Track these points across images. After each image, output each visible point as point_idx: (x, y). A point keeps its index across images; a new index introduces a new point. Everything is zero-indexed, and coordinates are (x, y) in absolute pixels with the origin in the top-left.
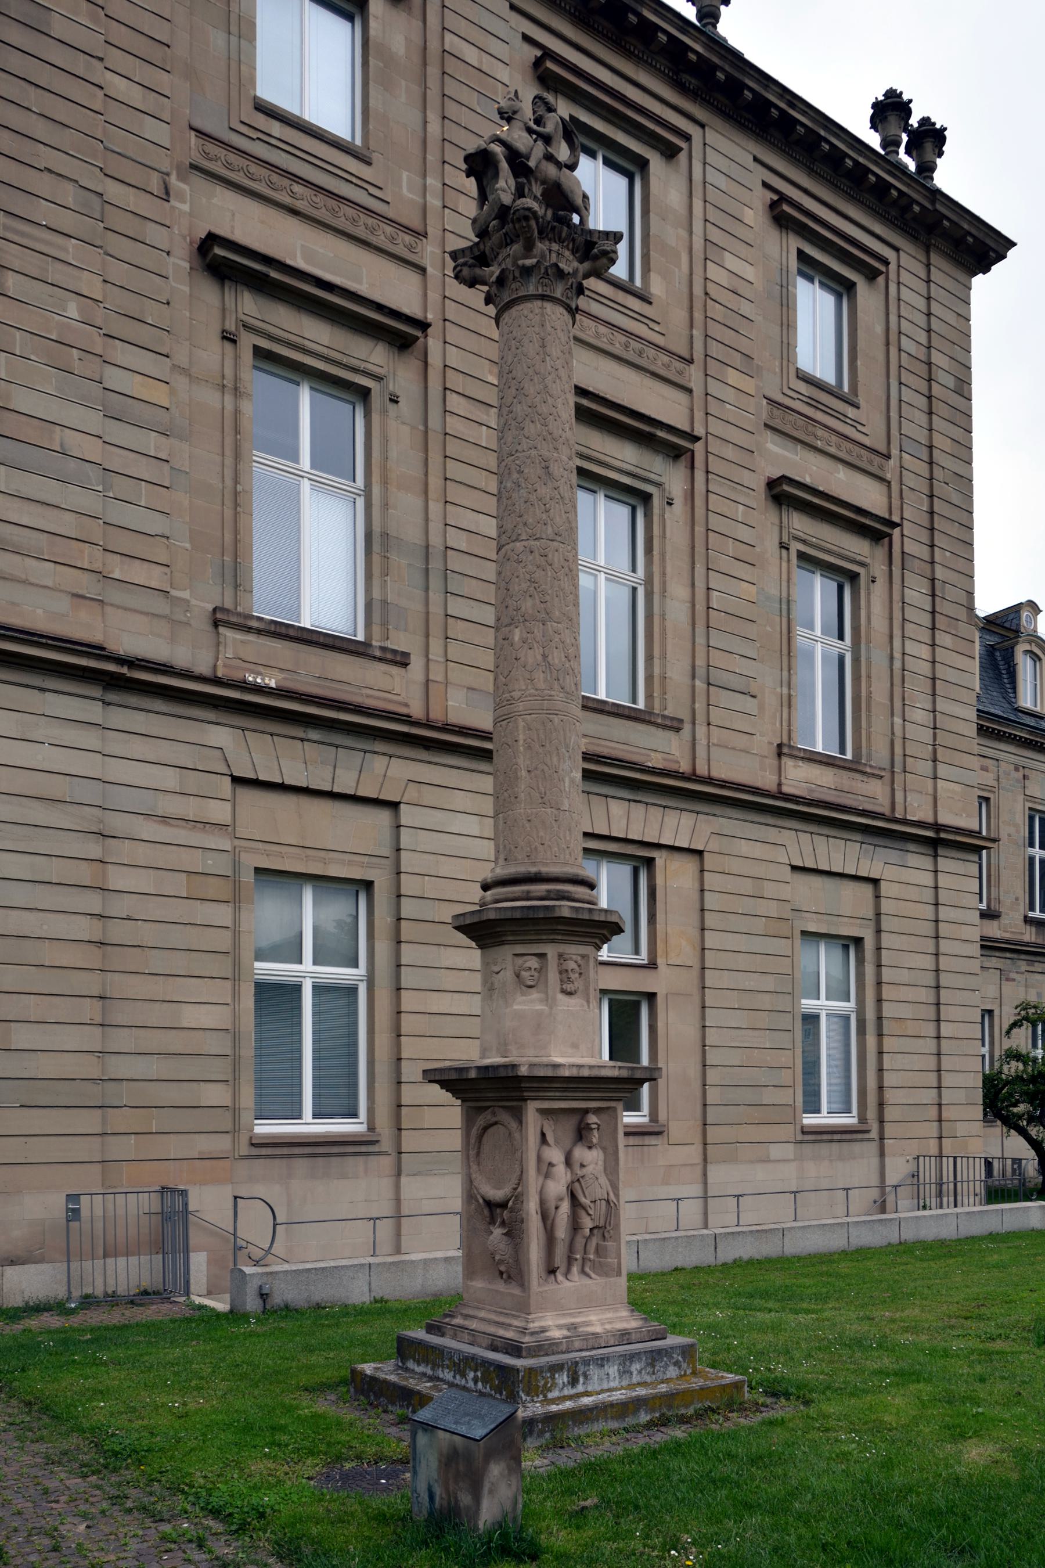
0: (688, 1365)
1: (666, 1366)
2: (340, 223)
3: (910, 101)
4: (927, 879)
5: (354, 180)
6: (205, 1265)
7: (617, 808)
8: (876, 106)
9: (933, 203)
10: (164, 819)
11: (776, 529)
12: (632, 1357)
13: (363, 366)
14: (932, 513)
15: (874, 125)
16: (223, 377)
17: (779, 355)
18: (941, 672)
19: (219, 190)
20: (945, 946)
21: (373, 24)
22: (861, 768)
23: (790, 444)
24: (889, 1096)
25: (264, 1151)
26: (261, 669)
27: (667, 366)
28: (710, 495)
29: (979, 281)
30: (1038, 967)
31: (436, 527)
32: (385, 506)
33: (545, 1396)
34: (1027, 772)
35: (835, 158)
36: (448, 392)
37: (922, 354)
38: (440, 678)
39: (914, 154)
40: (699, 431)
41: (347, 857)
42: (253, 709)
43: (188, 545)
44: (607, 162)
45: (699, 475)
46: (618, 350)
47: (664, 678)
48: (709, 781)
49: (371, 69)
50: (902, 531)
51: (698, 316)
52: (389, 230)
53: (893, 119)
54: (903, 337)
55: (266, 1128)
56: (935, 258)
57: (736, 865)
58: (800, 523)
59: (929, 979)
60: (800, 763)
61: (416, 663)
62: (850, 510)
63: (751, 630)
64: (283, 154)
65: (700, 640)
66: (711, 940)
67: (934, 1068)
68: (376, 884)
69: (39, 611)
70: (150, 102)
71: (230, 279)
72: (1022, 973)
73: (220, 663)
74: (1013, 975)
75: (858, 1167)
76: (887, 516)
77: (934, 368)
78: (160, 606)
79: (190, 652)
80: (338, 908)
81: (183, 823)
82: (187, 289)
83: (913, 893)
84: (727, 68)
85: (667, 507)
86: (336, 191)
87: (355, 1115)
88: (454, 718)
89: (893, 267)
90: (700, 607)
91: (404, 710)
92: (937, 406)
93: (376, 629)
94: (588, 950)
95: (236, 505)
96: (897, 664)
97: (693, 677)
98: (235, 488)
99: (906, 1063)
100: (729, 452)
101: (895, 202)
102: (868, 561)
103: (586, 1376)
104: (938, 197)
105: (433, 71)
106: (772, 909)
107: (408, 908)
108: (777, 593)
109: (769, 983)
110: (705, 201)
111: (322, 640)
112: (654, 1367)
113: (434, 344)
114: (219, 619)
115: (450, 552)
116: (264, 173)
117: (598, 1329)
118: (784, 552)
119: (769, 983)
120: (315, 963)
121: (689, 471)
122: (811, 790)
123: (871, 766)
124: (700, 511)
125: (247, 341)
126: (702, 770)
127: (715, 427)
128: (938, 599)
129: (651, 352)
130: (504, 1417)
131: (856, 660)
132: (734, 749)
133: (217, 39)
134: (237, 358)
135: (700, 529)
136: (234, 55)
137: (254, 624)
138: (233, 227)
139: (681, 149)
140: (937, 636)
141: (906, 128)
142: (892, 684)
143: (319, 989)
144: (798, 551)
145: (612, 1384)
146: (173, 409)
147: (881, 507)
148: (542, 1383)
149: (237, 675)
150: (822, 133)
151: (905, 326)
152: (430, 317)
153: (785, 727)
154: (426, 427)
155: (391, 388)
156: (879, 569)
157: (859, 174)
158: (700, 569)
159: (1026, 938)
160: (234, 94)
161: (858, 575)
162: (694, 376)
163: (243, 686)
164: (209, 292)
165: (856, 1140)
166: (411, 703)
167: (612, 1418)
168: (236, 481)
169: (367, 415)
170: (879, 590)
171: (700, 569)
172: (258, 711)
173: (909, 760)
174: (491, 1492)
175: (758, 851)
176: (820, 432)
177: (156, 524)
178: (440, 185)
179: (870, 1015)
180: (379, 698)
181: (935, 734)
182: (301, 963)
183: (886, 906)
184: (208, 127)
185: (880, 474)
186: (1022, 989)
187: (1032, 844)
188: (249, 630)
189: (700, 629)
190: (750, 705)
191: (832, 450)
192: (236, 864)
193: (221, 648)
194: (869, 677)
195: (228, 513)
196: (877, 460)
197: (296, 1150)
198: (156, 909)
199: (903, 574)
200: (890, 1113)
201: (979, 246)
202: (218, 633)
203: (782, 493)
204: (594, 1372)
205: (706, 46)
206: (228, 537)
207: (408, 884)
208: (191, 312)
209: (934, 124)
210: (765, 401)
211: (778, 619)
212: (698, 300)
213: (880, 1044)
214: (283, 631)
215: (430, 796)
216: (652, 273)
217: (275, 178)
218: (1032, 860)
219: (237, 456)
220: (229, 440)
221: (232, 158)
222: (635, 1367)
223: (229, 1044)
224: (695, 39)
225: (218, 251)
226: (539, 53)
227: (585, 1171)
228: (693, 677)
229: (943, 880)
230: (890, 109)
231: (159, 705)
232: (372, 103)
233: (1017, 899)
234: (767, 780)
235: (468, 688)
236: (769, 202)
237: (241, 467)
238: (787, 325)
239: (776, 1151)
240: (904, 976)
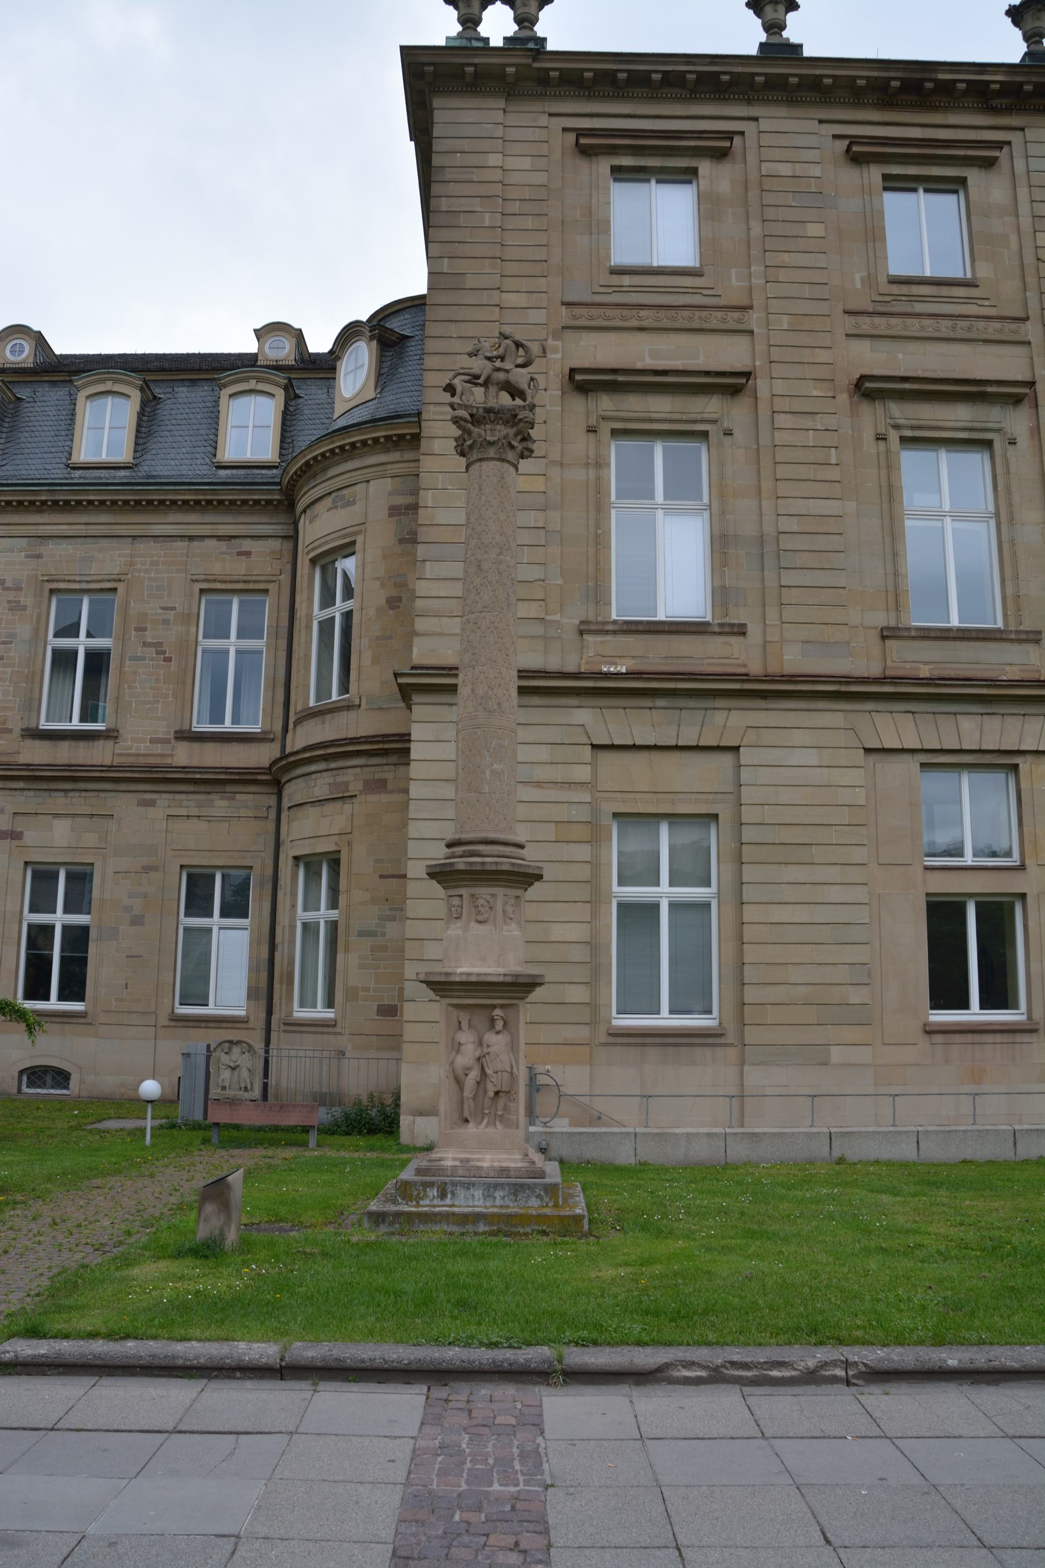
0: (550, 1199)
1: (528, 1197)
5: (690, 290)
7: (967, 724)
10: (539, 784)
12: (496, 1186)
16: (588, 458)
19: (584, 335)
21: (701, 183)
25: (620, 1040)
26: (617, 660)
33: (418, 1202)
41: (693, 796)
44: (926, 191)
46: (945, 333)
61: (754, 632)
68: (720, 816)
69: (450, 652)
71: (592, 391)
78: (538, 630)
80: (689, 835)
85: (1011, 448)
86: (676, 304)
87: (710, 1012)
88: (789, 669)
94: (518, 892)
95: (597, 544)
103: (453, 1194)
105: (753, 194)
112: (517, 1196)
114: (584, 630)
115: (781, 536)
116: (617, 312)
117: (485, 1165)
120: (671, 885)
121: (1033, 410)
125: (606, 428)
129: (981, 324)
130: (215, 1179)
137: (610, 627)
143: (673, 906)
145: (476, 1203)
148: (415, 1193)
149: (595, 668)
154: (758, 444)
155: (725, 425)
167: (453, 1223)
174: (205, 1220)
178: (763, 268)
182: (658, 885)
188: (607, 632)
192: (596, 812)
197: (648, 1040)
204: (461, 1192)
205: (1006, 73)
206: (591, 568)
207: (748, 814)
214: (634, 628)
215: (768, 737)
222: (499, 1194)
227: (489, 1050)
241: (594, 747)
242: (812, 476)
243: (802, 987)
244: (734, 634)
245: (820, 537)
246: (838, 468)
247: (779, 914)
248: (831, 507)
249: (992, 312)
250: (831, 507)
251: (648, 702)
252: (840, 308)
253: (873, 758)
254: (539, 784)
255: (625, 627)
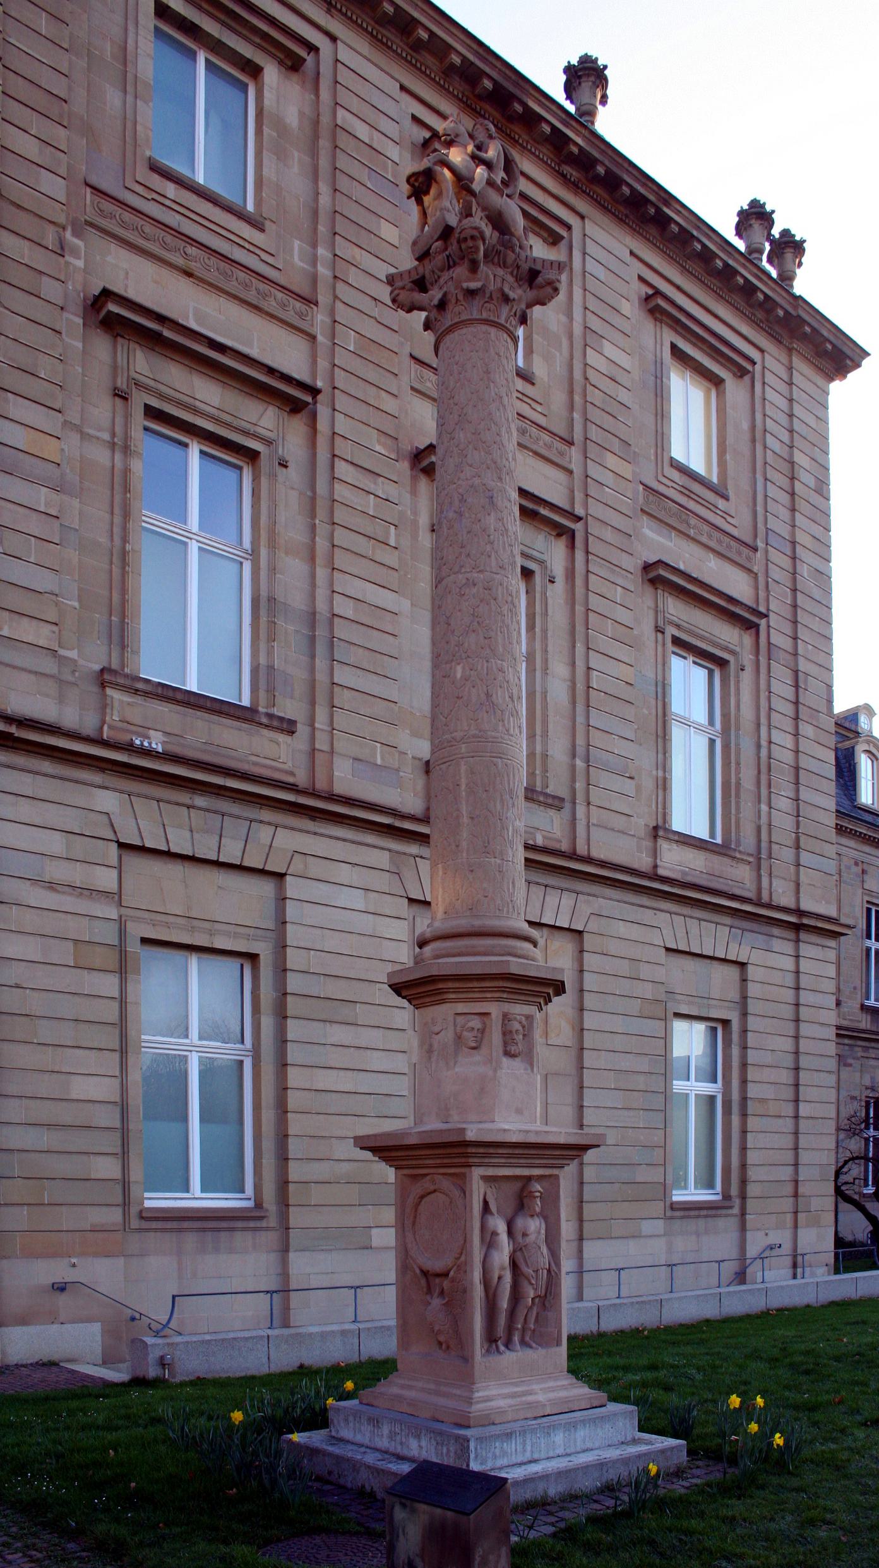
2: (232, 287)
3: (773, 212)
4: (788, 964)
5: (246, 245)
6: (99, 1336)
8: (742, 213)
9: (796, 307)
10: (51, 886)
11: (651, 614)
13: (252, 429)
14: (795, 606)
15: (739, 232)
17: (653, 442)
18: (804, 762)
20: (804, 1029)
22: (733, 854)
23: (665, 531)
24: (752, 1174)
25: (154, 1225)
27: (549, 447)
28: (590, 575)
29: (836, 388)
30: (872, 1053)
31: (321, 593)
32: (273, 570)
34: (865, 867)
35: (706, 256)
36: (336, 459)
37: (784, 451)
38: (326, 748)
39: (776, 261)
40: (579, 511)
42: (139, 773)
43: (76, 604)
45: (579, 555)
47: (545, 756)
48: (589, 860)
49: (265, 140)
50: (768, 622)
51: (577, 398)
52: (279, 295)
53: (756, 225)
54: (768, 435)
55: (156, 1200)
56: (797, 362)
57: (613, 947)
58: (675, 608)
59: (789, 1061)
60: (674, 846)
61: (302, 729)
62: (720, 598)
63: (629, 712)
64: (178, 217)
65: (580, 719)
66: (589, 1021)
67: (791, 1145)
68: (262, 957)
70: (45, 156)
72: (858, 1059)
73: (105, 728)
74: (850, 1061)
75: (720, 1242)
76: (754, 606)
77: (796, 467)
78: (48, 665)
79: (73, 713)
81: (67, 889)
82: (80, 345)
83: (777, 977)
84: (607, 163)
85: (549, 585)
88: (339, 789)
89: (758, 367)
90: (580, 686)
91: (291, 780)
92: (801, 505)
93: (262, 694)
96: (764, 752)
97: (574, 756)
98: (124, 548)
99: (767, 1141)
100: (608, 535)
101: (761, 305)
102: (738, 649)
104: (801, 303)
105: (324, 143)
106: (648, 991)
107: (294, 983)
108: (653, 676)
109: (643, 1065)
110: (585, 290)
111: (209, 705)
113: (323, 411)
114: (105, 678)
115: (336, 620)
118: (659, 635)
119: (643, 1065)
122: (684, 873)
123: (740, 852)
124: (579, 590)
125: (140, 399)
126: (581, 849)
127: (595, 509)
128: (801, 690)
131: (726, 747)
132: (613, 829)
133: (113, 98)
134: (127, 417)
135: (580, 609)
136: (129, 115)
137: (140, 686)
138: (126, 286)
139: (563, 238)
140: (801, 727)
141: (769, 237)
142: (759, 772)
144: (673, 636)
146: (64, 465)
147: (749, 603)
149: (124, 738)
150: (695, 233)
151: (770, 424)
152: (319, 384)
153: (660, 810)
155: (280, 452)
156: (747, 658)
157: (728, 273)
158: (580, 648)
159: (863, 1026)
160: (129, 154)
161: (727, 662)
162: (574, 457)
163: (129, 748)
164: (102, 345)
165: (720, 1216)
166: (296, 771)
168: (125, 540)
169: (256, 479)
170: (747, 677)
171: (580, 648)
172: (145, 775)
173: (774, 846)
175: (635, 932)
176: (693, 521)
177: (43, 581)
178: (331, 256)
179: (735, 1096)
180: (265, 766)
181: (798, 823)
183: (753, 990)
184: (104, 186)
185: (748, 565)
186: (858, 1074)
187: (869, 937)
188: (136, 691)
189: (580, 708)
190: (629, 787)
191: (704, 539)
192: (122, 933)
193: (108, 711)
194: (738, 764)
195: (116, 571)
196: (745, 551)
197: (186, 1224)
198: (43, 978)
199: (769, 664)
200: (752, 1190)
201: (837, 355)
202: (105, 695)
203: (658, 576)
207: (294, 959)
208: (83, 368)
209: (794, 236)
210: (641, 487)
211: (653, 702)
212: (577, 386)
213: (744, 1124)
214: (170, 694)
215: (316, 868)
216: (535, 355)
217: (169, 239)
218: (868, 950)
219: (126, 515)
220: (118, 498)
221: (127, 216)
223: (118, 1116)
224: (578, 133)
225: (113, 307)
226: (428, 135)
228: (574, 756)
229: (804, 965)
230: (755, 216)
231: (46, 766)
232: (266, 172)
233: (855, 988)
234: (643, 862)
235: (355, 759)
236: (644, 296)
237: (130, 525)
238: (662, 415)
239: (647, 1227)
240: (768, 1058)
241: (122, 846)
242: (370, 554)
243: (345, 1164)
244: (282, 731)
245: (376, 633)
246: (396, 553)
247: (325, 1080)
248: (386, 599)
249: (542, 421)
250: (386, 599)
251: (184, 797)
252: (407, 350)
253: (672, 955)
254: (51, 886)
255: (160, 691)
